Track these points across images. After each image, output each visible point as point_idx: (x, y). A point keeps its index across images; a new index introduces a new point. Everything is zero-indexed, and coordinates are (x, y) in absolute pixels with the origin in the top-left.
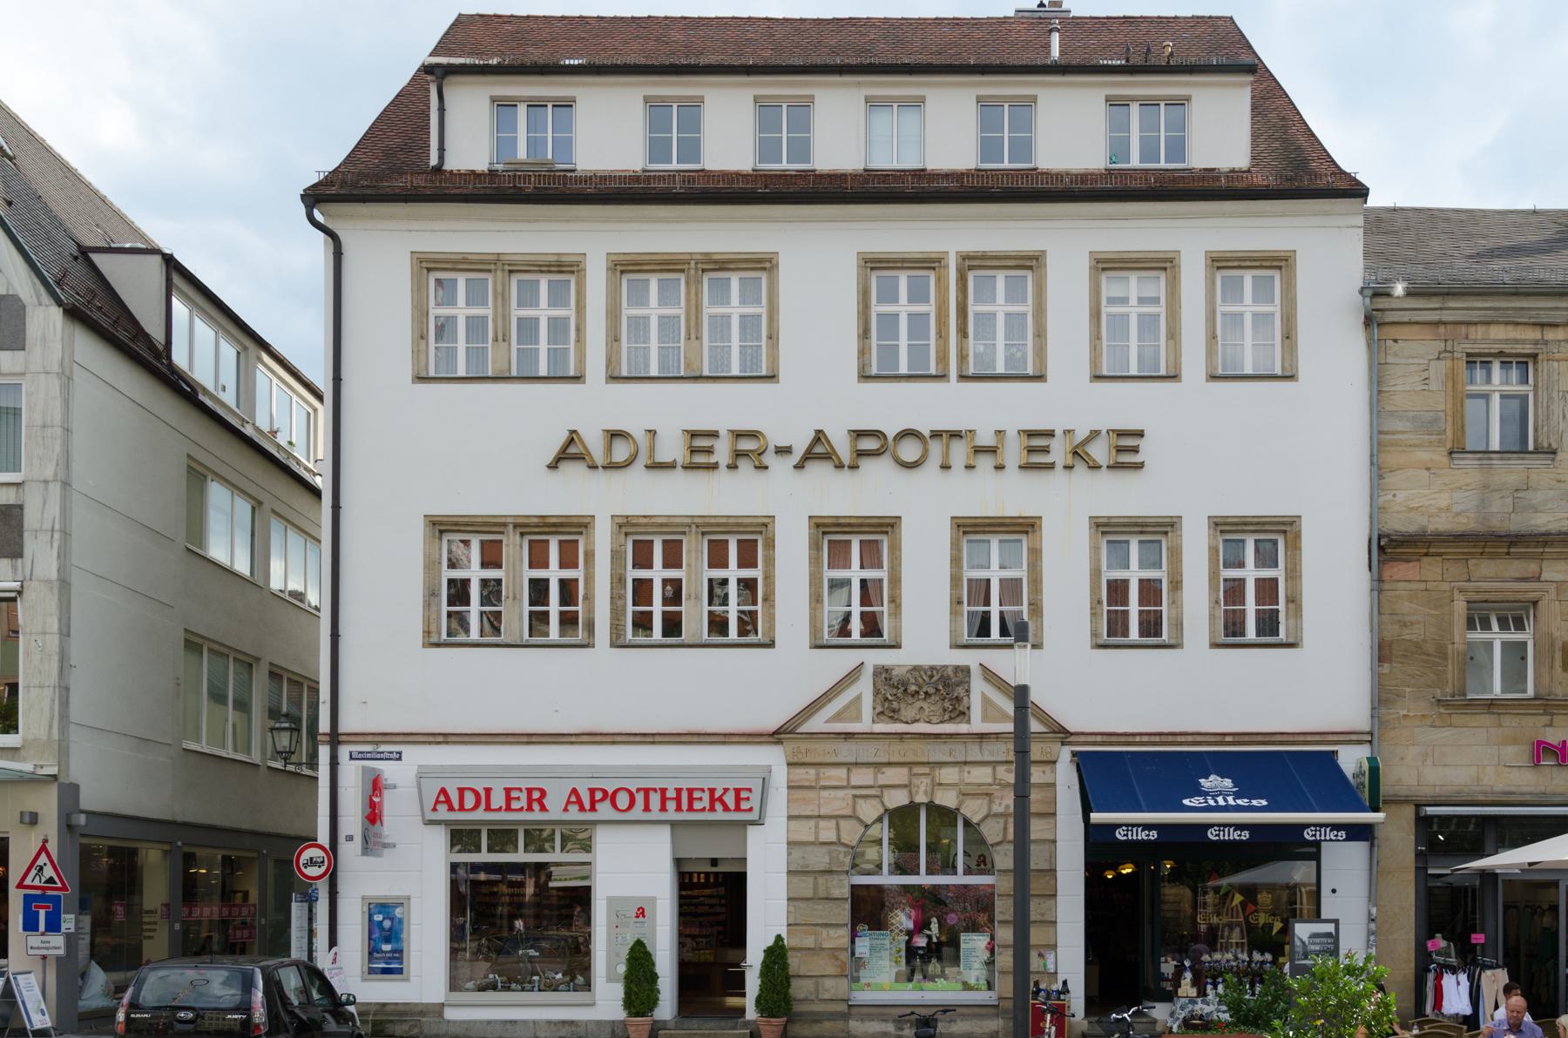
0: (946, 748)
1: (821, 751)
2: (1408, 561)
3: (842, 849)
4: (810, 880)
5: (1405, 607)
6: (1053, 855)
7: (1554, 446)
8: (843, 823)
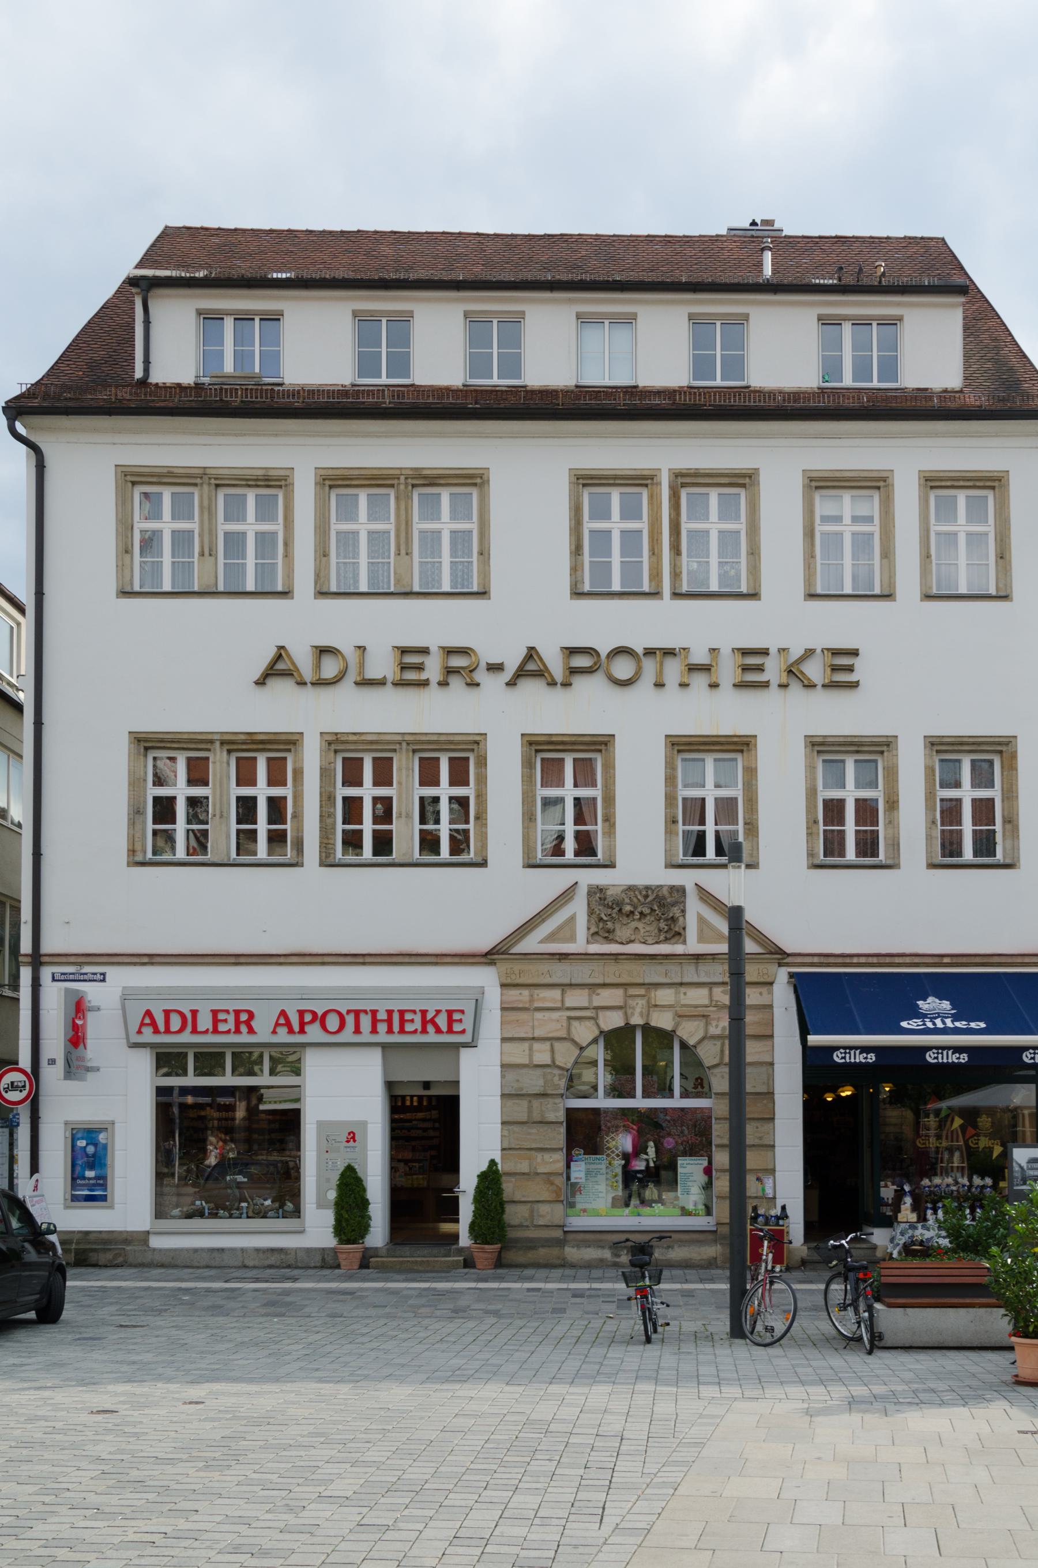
0: (661, 969)
3: (557, 1072)
4: (524, 1103)
6: (771, 1078)
8: (557, 1045)
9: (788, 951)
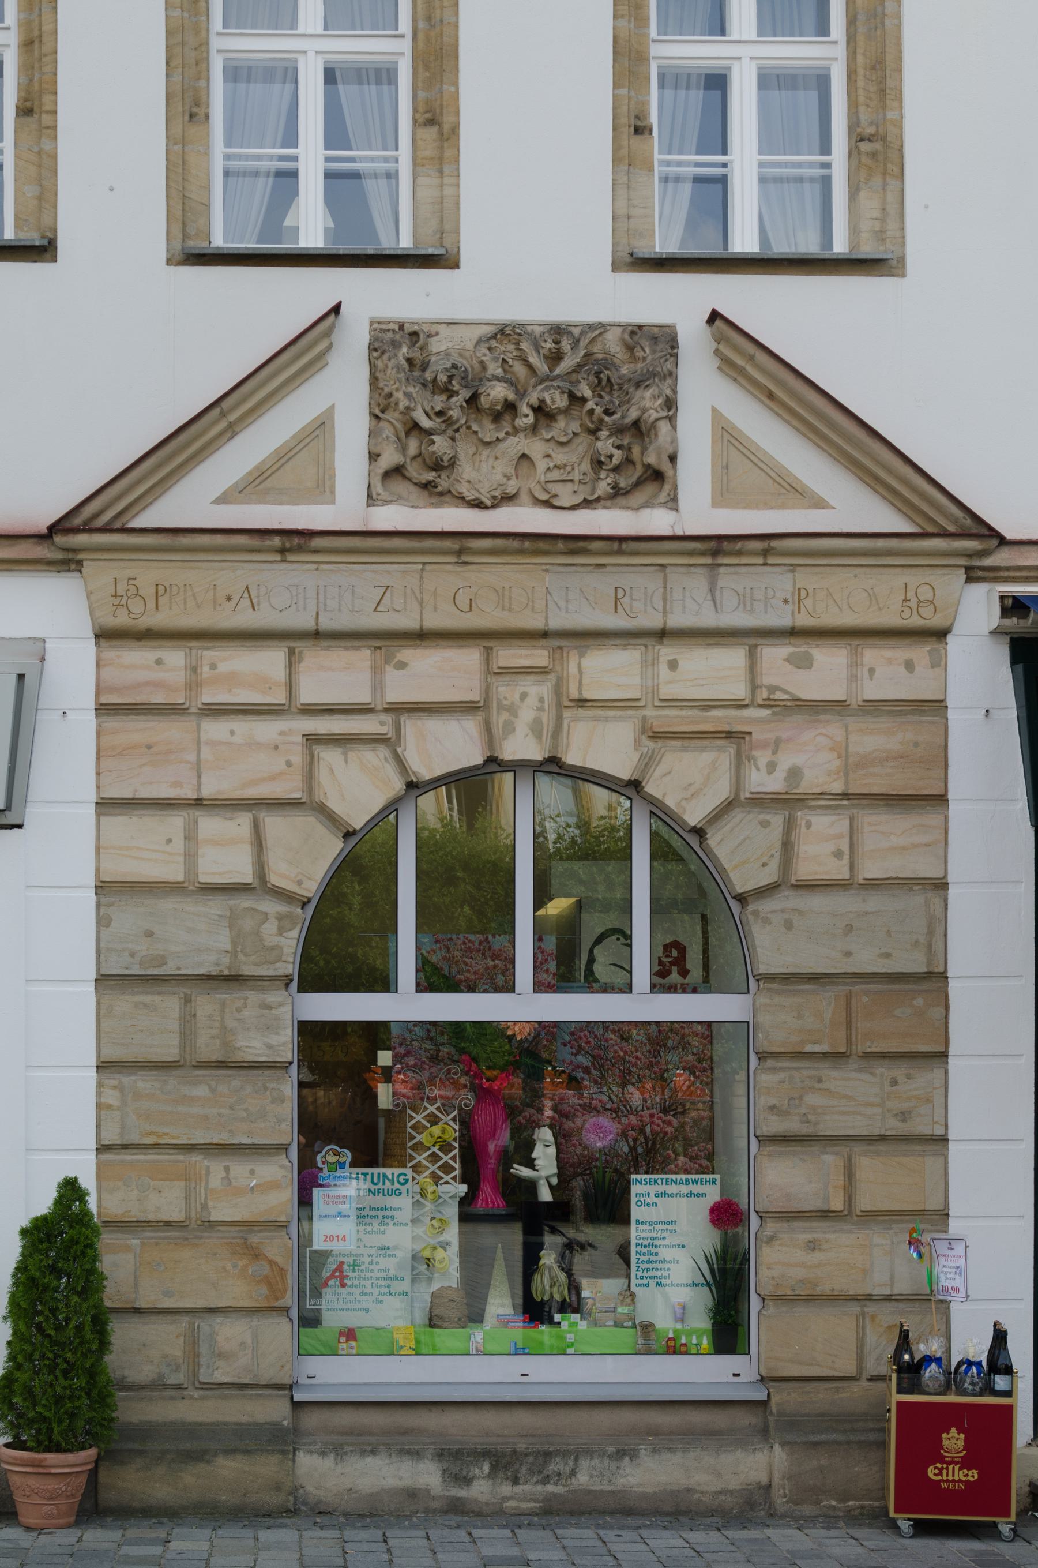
0: (602, 584)
1: (204, 592)
3: (272, 907)
4: (170, 1004)
6: (937, 929)
8: (274, 825)
9: (1009, 535)
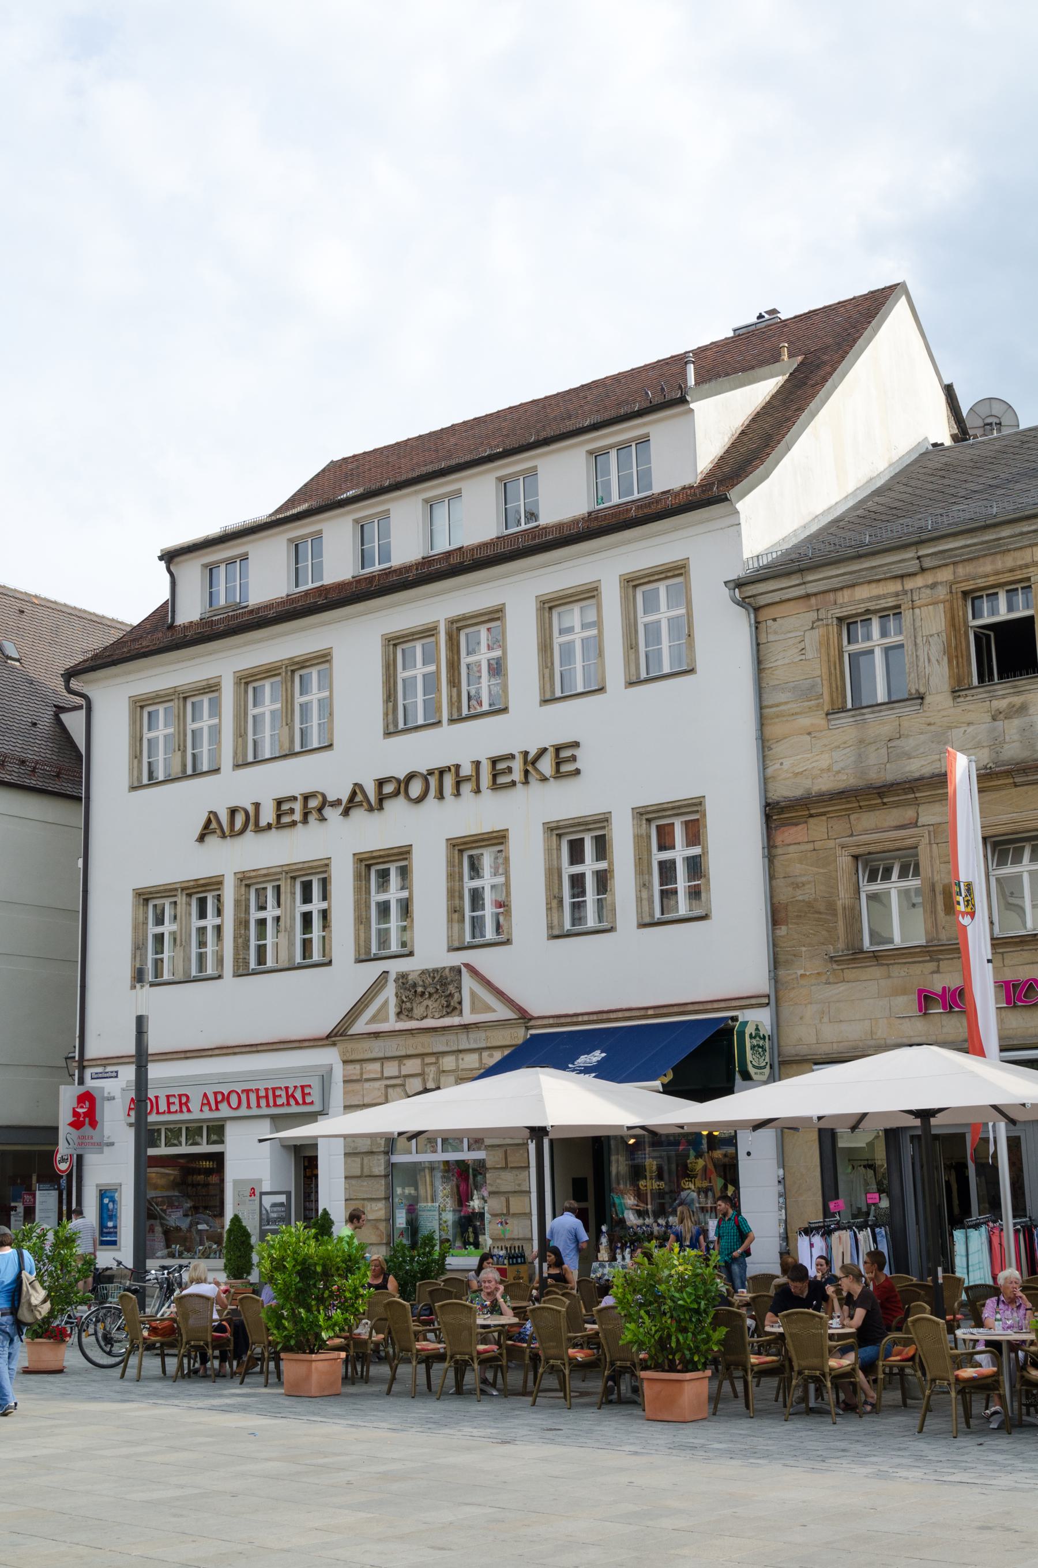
0: (443, 1039)
2: (796, 825)
4: (358, 1160)
5: (797, 868)
7: (922, 690)
